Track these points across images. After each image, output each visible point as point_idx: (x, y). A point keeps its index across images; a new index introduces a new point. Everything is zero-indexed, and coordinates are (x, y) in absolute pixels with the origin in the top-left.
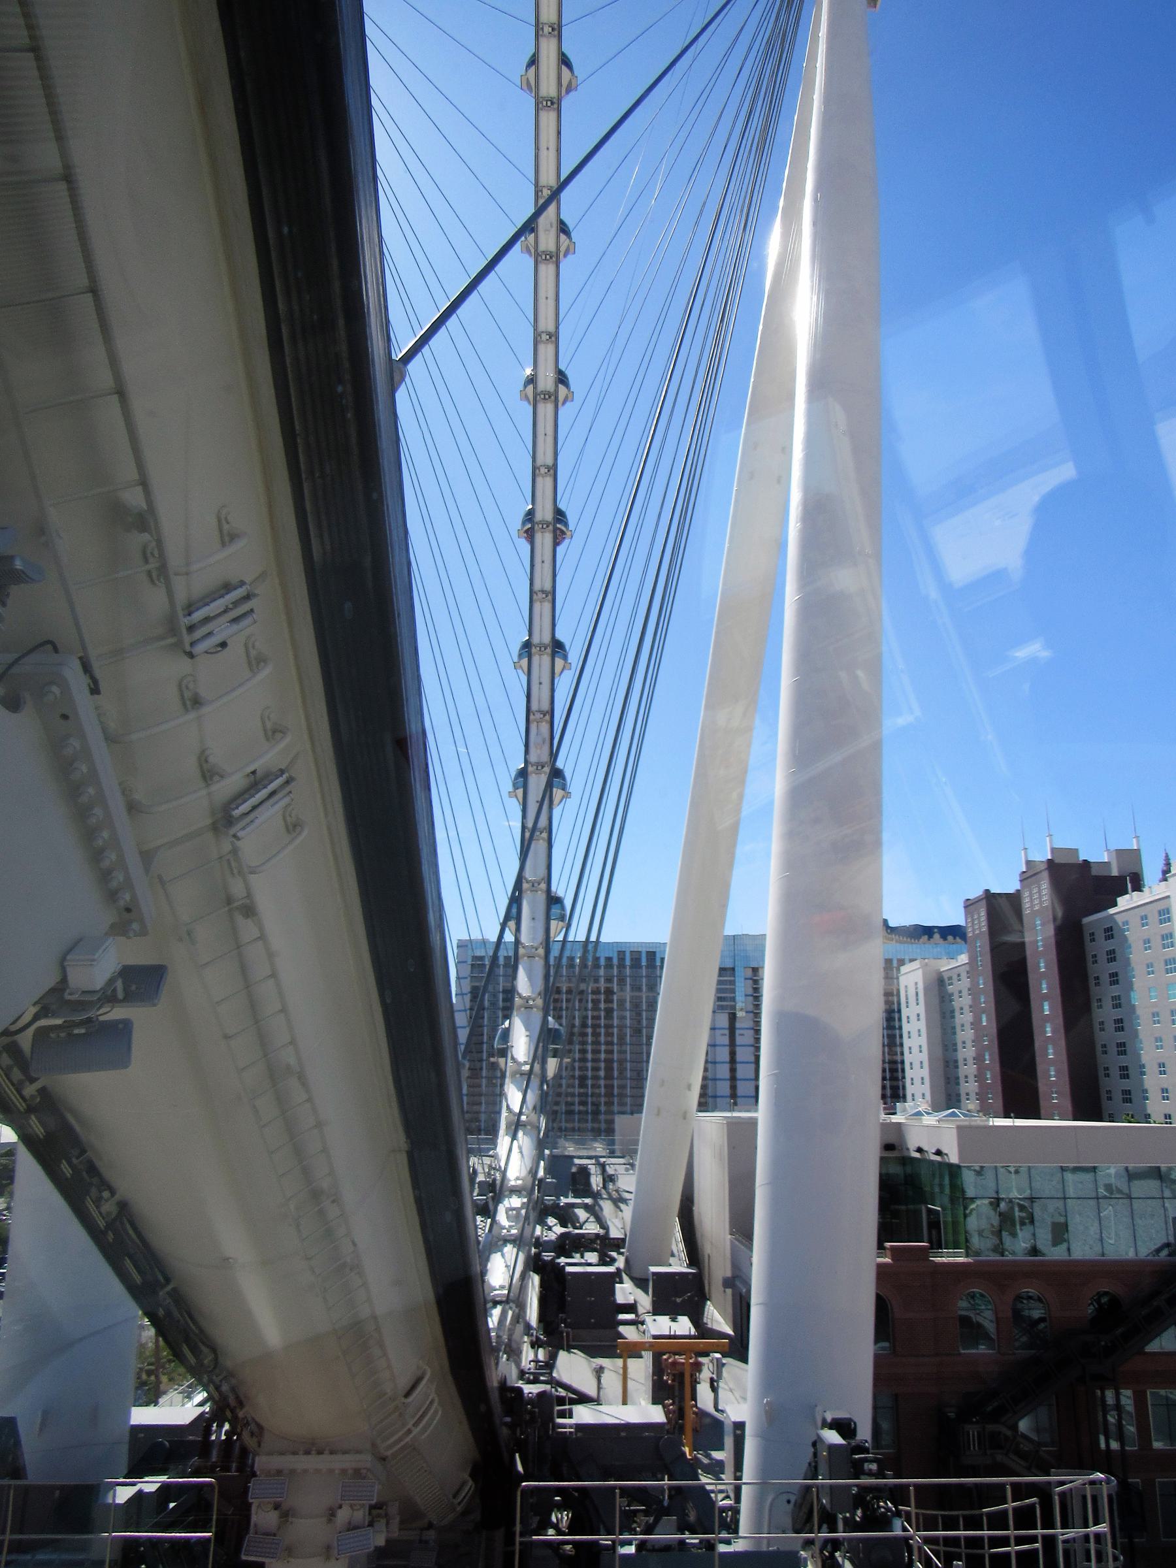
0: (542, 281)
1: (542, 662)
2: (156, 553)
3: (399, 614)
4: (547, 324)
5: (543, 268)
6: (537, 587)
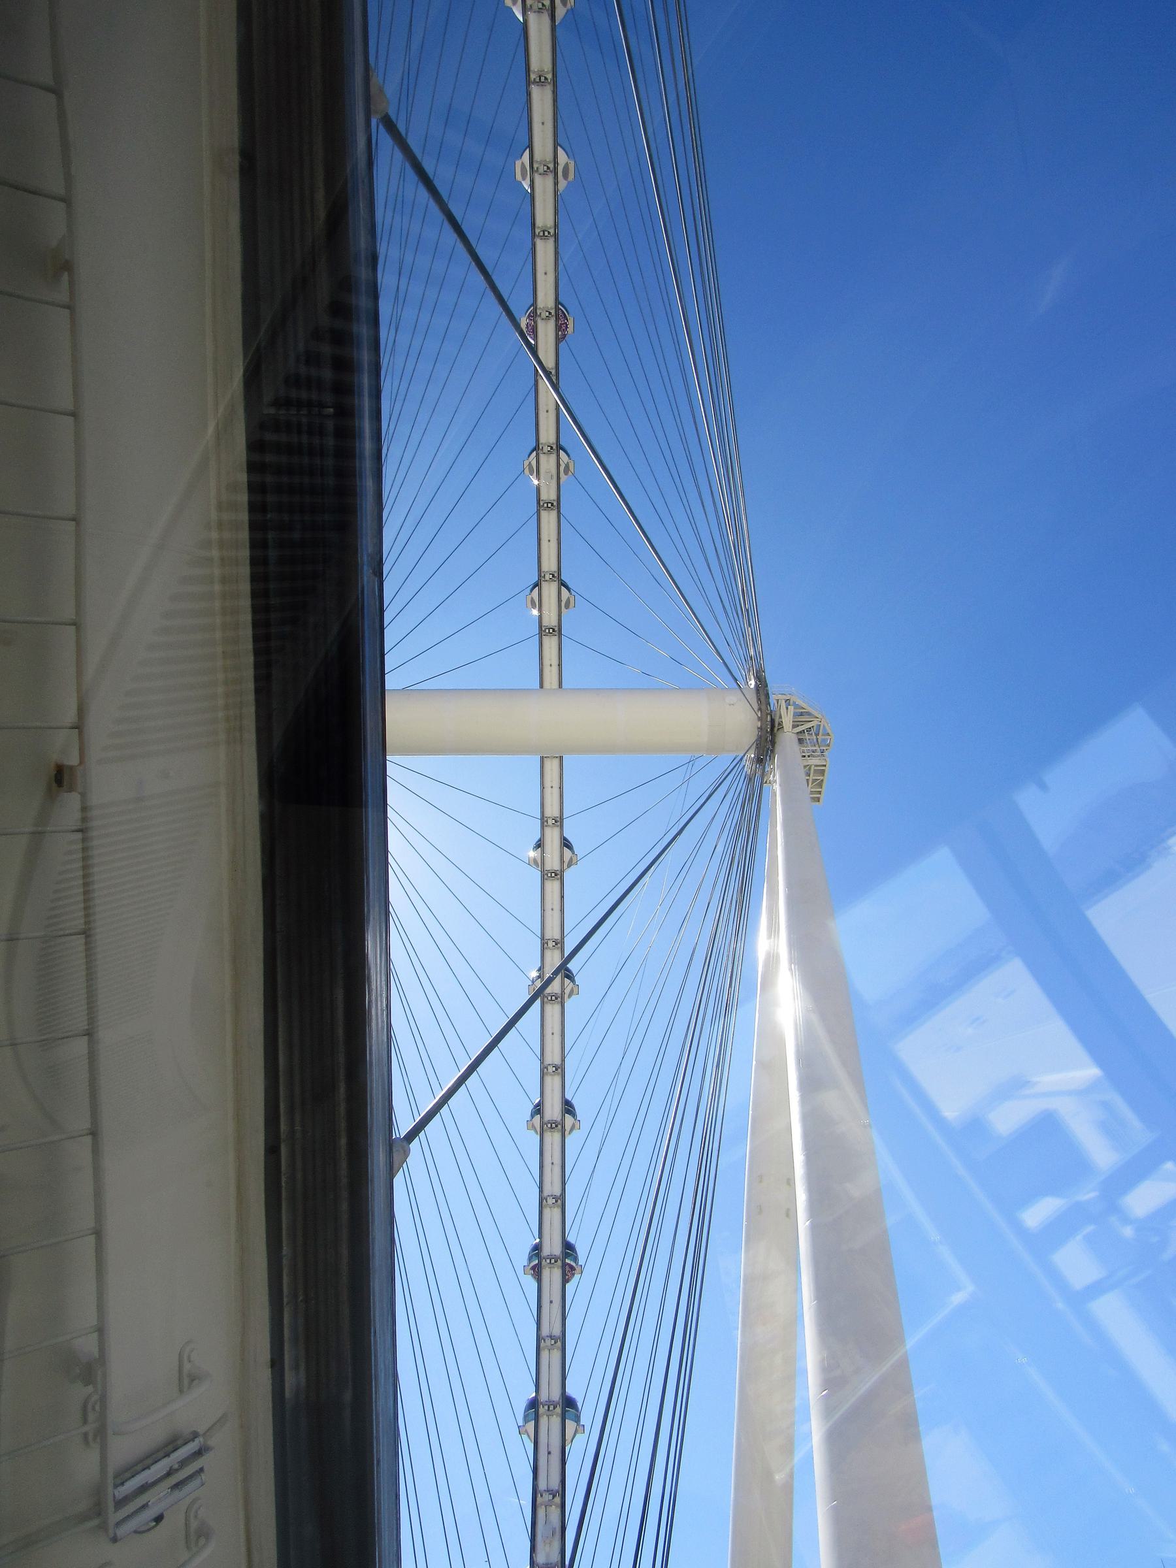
0: (547, 1147)
1: (551, 1424)
2: (97, 1408)
3: (378, 1461)
4: (553, 1057)
5: (548, 884)
6: (545, 1332)
